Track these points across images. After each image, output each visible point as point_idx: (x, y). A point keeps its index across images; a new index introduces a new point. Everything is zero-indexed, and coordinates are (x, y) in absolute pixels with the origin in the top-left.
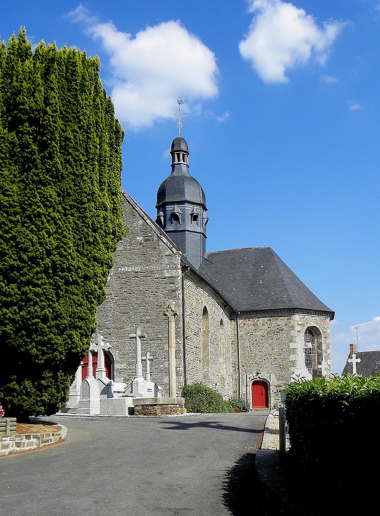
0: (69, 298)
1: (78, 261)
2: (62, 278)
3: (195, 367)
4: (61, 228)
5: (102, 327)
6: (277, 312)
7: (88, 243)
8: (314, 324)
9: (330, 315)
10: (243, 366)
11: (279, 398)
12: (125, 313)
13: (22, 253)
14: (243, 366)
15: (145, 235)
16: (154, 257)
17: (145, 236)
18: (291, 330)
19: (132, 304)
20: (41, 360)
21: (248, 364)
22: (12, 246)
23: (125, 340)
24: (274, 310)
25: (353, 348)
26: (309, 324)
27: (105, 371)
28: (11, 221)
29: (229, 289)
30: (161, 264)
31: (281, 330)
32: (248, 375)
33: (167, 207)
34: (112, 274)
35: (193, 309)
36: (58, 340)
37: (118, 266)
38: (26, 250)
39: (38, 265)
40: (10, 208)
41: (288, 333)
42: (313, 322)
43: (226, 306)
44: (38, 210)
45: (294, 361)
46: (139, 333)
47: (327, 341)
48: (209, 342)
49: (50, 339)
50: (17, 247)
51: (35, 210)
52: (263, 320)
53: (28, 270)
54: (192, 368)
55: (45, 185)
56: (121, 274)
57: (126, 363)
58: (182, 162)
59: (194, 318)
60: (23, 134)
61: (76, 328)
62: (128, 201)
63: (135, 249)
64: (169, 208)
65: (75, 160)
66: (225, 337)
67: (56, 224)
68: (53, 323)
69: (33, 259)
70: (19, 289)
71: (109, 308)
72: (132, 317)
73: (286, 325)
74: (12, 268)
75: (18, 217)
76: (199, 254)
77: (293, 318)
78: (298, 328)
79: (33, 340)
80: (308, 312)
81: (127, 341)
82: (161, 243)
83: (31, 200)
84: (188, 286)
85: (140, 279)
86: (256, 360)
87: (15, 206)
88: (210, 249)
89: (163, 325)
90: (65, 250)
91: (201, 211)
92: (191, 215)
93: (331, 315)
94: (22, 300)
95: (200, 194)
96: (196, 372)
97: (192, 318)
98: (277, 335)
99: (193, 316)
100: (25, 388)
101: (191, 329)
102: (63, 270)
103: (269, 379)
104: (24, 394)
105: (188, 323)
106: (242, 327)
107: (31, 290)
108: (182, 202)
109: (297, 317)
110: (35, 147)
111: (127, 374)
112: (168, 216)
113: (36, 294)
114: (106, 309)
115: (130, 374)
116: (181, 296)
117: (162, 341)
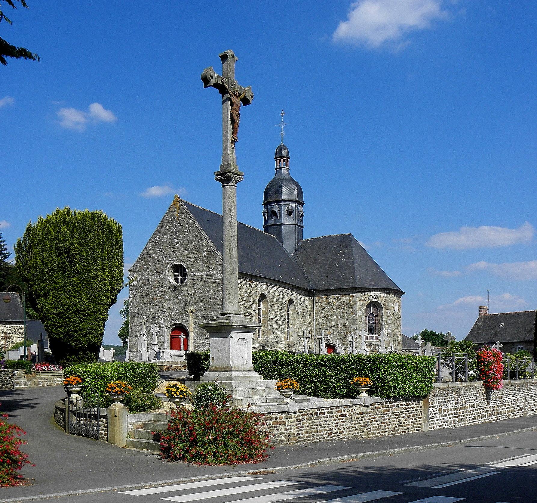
0: (87, 322)
1: (89, 305)
2: (82, 314)
4: (80, 294)
7: (96, 298)
8: (375, 299)
10: (317, 333)
12: (196, 303)
13: (63, 307)
14: (317, 333)
18: (354, 305)
20: (76, 347)
22: (60, 304)
24: (341, 290)
25: (482, 310)
26: (370, 300)
28: (59, 294)
29: (311, 271)
30: (216, 270)
33: (269, 205)
34: (188, 277)
36: (83, 339)
38: (65, 305)
39: (71, 310)
40: (58, 289)
42: (374, 298)
44: (69, 289)
46: (166, 325)
47: (388, 313)
49: (79, 339)
50: (61, 304)
51: (68, 289)
52: (333, 297)
53: (67, 313)
55: (72, 277)
60: (62, 258)
61: (90, 333)
62: (197, 228)
63: (201, 260)
64: (270, 206)
65: (87, 263)
67: (78, 292)
68: (80, 332)
69: (68, 309)
70: (64, 320)
73: (350, 301)
74: (60, 313)
75: (62, 292)
76: (295, 242)
78: (360, 303)
79: (72, 340)
82: (216, 256)
83: (67, 285)
86: (327, 329)
87: (60, 288)
88: (307, 236)
90: (82, 303)
92: (287, 210)
93: (398, 293)
94: (66, 325)
100: (73, 359)
102: (82, 311)
103: (336, 344)
104: (73, 361)
107: (68, 321)
108: (280, 201)
109: (359, 295)
110: (67, 263)
112: (270, 213)
113: (71, 322)
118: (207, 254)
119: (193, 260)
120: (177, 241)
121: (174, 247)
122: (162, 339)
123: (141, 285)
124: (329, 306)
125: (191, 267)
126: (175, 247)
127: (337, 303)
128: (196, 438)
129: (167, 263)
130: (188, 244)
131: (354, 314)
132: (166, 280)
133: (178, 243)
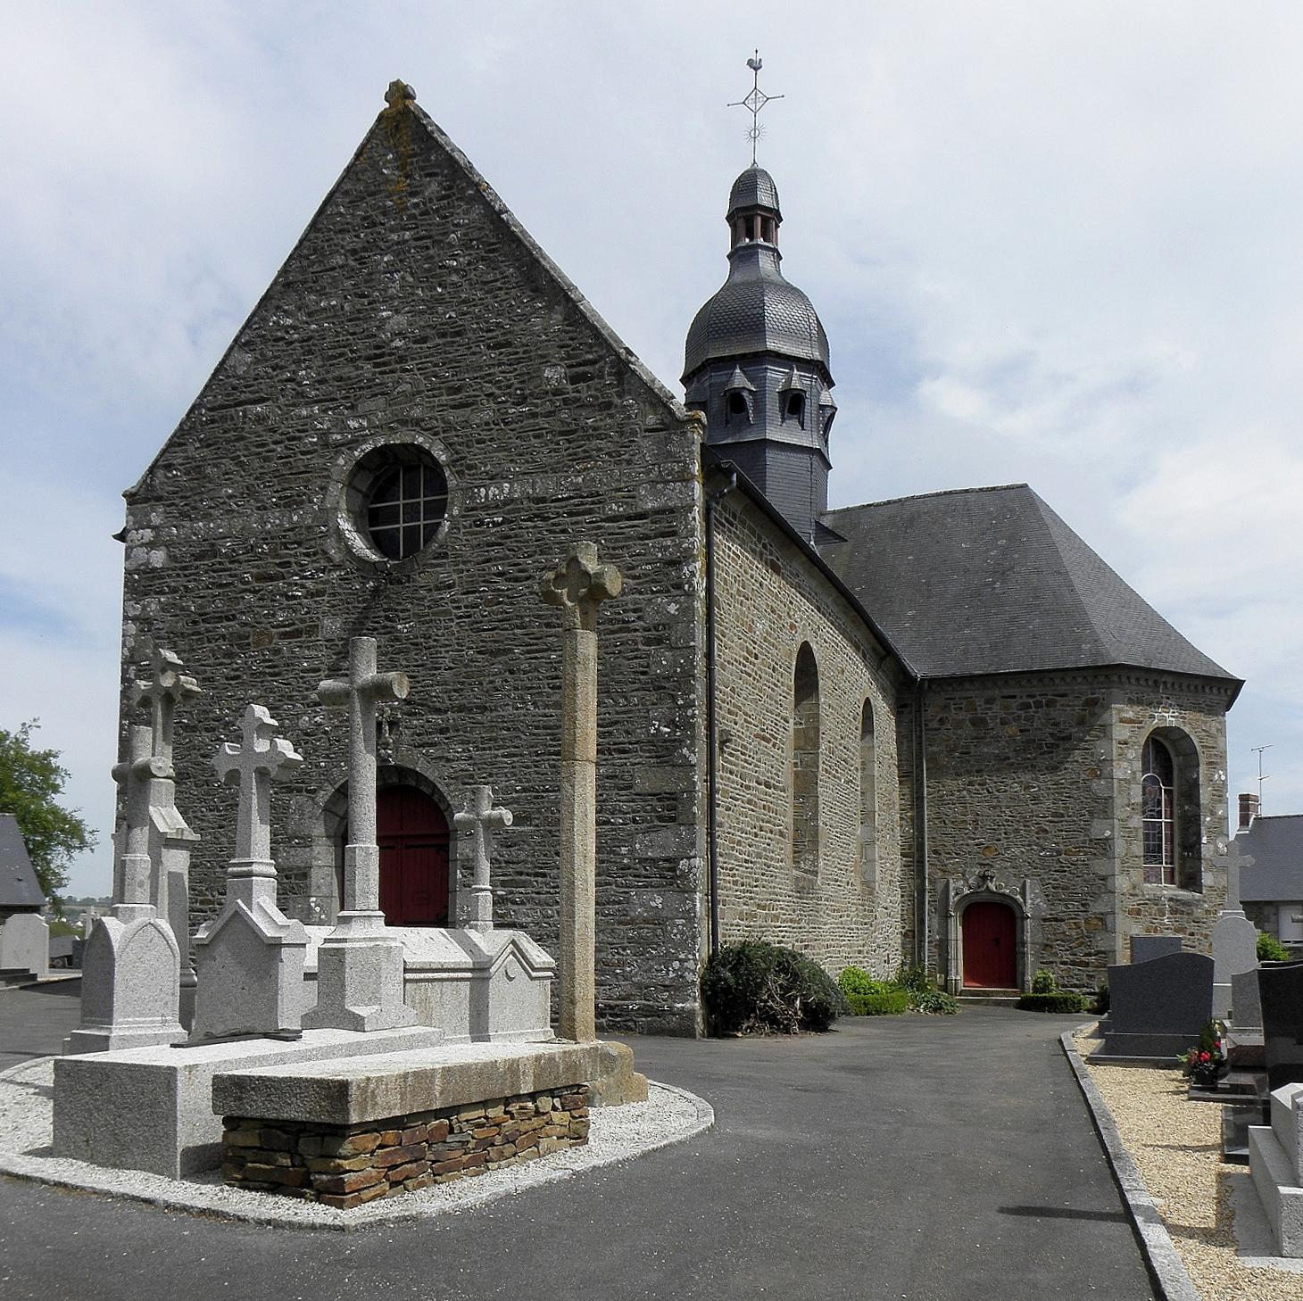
3: (759, 856)
5: (419, 705)
6: (1051, 679)
9: (1226, 690)
10: (935, 852)
11: (1051, 960)
15: (572, 360)
16: (602, 439)
17: (574, 362)
19: (522, 617)
21: (953, 848)
23: (496, 752)
27: (273, 871)
31: (1063, 739)
32: (951, 881)
34: (456, 512)
35: (756, 643)
37: (476, 479)
41: (1087, 749)
43: (882, 659)
45: (1107, 839)
47: (1216, 776)
48: (820, 769)
54: (746, 861)
56: (485, 507)
57: (499, 837)
58: (761, 241)
59: (757, 677)
63: (534, 415)
66: (878, 758)
71: (444, 635)
72: (522, 667)
77: (1104, 699)
80: (1155, 682)
81: (503, 756)
84: (734, 553)
85: (554, 525)
89: (633, 694)
91: (814, 383)
95: (813, 331)
96: (763, 874)
97: (750, 675)
98: (1050, 755)
99: (755, 669)
101: (746, 714)
105: (733, 690)
106: (936, 729)
111: (502, 878)
114: (435, 640)
115: (510, 878)
116: (700, 584)
117: (626, 756)
118: (574, 380)
119: (487, 415)
120: (400, 321)
121: (377, 356)
122: (297, 858)
123: (185, 568)
124: (988, 745)
125: (474, 455)
126: (382, 355)
127: (1021, 731)
128: (193, 558)
129: (338, 446)
130: (458, 334)
131: (1099, 777)
132: (325, 536)
133: (401, 335)
